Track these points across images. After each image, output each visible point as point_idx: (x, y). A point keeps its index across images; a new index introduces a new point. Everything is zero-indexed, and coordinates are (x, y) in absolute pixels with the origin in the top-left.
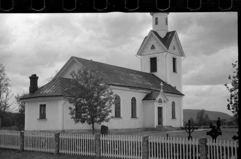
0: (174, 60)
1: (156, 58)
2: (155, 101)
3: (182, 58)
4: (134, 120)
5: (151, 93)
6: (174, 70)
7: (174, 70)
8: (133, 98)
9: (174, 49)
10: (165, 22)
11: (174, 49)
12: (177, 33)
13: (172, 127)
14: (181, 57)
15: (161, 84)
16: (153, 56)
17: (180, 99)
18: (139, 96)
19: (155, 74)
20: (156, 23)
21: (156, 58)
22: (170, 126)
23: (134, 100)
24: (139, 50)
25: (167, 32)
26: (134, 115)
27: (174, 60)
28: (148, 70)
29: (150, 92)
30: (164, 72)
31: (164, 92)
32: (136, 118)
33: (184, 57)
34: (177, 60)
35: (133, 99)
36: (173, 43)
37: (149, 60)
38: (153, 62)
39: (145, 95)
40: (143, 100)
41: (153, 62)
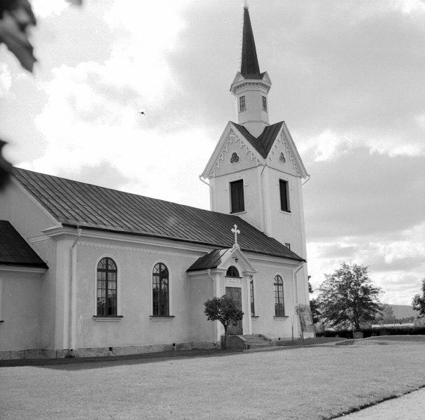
0: (283, 184)
1: (241, 181)
2: (215, 271)
3: (303, 180)
4: (162, 323)
5: (212, 253)
6: (285, 206)
7: (285, 206)
8: (230, 268)
9: (282, 159)
10: (261, 104)
11: (282, 159)
12: (286, 127)
13: (265, 339)
14: (299, 179)
15: (232, 230)
16: (236, 178)
17: (295, 270)
18: (178, 261)
19: (241, 216)
20: (242, 107)
21: (241, 181)
22: (260, 336)
23: (163, 274)
24: (207, 166)
25: (264, 126)
26: (160, 307)
27: (283, 184)
28: (226, 208)
29: (209, 252)
30: (262, 210)
31: (242, 250)
32: (168, 316)
33: (307, 177)
34: (290, 186)
35: (232, 271)
36: (277, 147)
37: (228, 187)
38: (237, 188)
39: (197, 257)
40: (189, 271)
41: (237, 188)
